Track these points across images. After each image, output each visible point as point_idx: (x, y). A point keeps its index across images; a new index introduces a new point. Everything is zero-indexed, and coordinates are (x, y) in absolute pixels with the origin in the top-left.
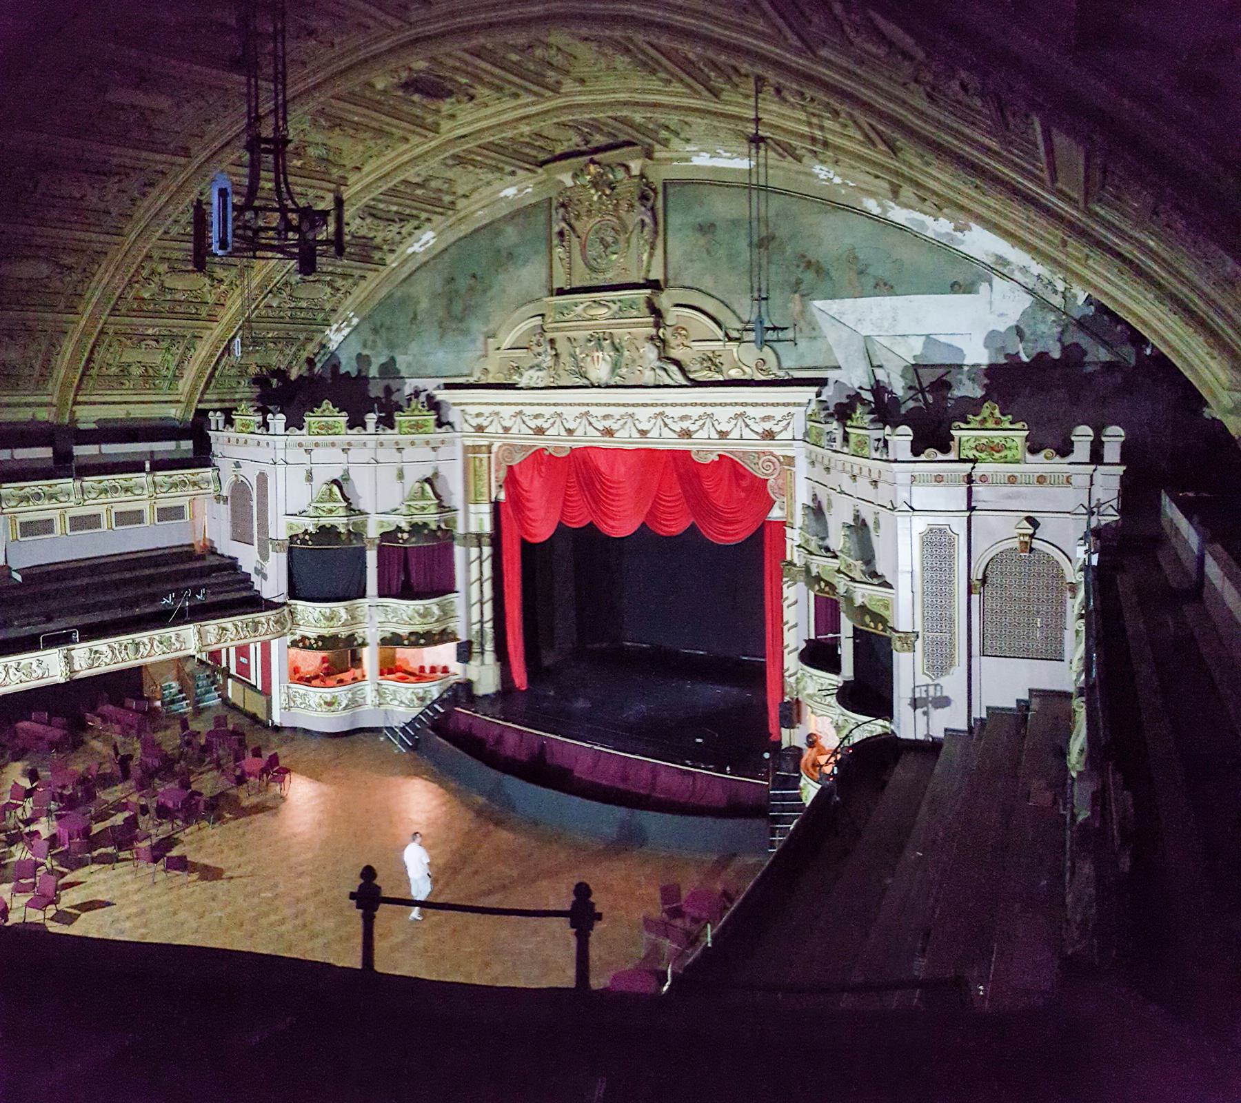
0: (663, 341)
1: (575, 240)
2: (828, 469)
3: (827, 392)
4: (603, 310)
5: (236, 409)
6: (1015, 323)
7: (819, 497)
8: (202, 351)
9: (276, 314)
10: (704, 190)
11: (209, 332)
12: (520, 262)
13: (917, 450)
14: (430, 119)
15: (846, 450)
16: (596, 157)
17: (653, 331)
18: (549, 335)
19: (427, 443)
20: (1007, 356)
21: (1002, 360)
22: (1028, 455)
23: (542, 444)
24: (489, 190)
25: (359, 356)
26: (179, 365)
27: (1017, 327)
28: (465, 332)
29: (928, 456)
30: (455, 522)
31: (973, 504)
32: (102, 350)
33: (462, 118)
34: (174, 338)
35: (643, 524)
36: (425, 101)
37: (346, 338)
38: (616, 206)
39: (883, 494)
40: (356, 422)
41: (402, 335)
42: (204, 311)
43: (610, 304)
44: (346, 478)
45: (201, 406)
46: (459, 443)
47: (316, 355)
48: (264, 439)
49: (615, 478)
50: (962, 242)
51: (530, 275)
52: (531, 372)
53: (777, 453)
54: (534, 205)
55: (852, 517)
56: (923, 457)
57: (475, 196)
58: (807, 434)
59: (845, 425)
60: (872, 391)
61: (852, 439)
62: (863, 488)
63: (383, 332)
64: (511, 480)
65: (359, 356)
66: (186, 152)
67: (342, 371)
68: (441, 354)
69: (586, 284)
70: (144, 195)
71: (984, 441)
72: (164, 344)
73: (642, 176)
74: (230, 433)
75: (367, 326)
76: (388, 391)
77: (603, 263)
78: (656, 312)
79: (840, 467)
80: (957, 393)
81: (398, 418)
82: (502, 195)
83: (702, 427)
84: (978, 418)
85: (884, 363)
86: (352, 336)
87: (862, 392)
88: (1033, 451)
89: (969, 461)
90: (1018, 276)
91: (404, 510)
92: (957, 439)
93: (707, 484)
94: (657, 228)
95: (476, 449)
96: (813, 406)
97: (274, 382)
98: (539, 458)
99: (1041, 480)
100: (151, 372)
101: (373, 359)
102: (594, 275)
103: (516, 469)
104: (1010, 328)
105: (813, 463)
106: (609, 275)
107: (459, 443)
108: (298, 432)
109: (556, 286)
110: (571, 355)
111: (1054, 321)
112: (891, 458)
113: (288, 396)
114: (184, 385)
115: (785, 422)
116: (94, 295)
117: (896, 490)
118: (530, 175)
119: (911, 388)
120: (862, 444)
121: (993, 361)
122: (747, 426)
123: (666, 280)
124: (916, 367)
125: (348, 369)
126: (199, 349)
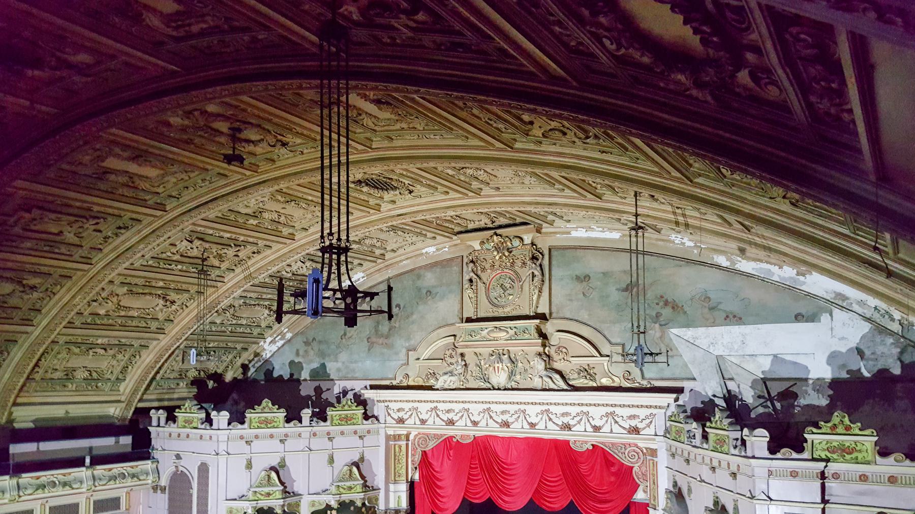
0: (549, 356)
1: (480, 285)
2: (688, 461)
3: (684, 398)
4: (503, 334)
5: (179, 407)
6: (853, 345)
7: (679, 484)
8: (147, 358)
9: (219, 329)
10: (580, 253)
11: (155, 343)
12: (437, 298)
13: (773, 448)
14: (372, 202)
15: (705, 446)
16: (499, 231)
17: (541, 349)
18: (460, 351)
19: (355, 432)
20: (848, 372)
21: (844, 375)
22: (878, 457)
23: (450, 433)
24: (413, 247)
25: (292, 363)
26: (124, 370)
27: (857, 348)
28: (390, 346)
29: (784, 454)
30: (377, 499)
31: (826, 498)
32: (49, 357)
33: (399, 204)
34: (121, 347)
35: (531, 501)
36: (372, 191)
37: (279, 349)
38: (513, 263)
39: (742, 485)
40: (293, 416)
41: (333, 347)
42: (154, 325)
43: (509, 330)
44: (283, 464)
45: (141, 405)
46: (382, 432)
47: (250, 362)
48: (207, 433)
49: (509, 461)
50: (804, 283)
51: (446, 307)
52: (446, 377)
53: (641, 445)
54: (452, 259)
55: (712, 503)
56: (779, 455)
57: (401, 251)
58: (667, 431)
59: (704, 426)
60: (724, 398)
61: (711, 437)
62: (722, 478)
63: (315, 344)
64: (425, 463)
65: (292, 363)
66: (161, 207)
67: (275, 375)
68: (368, 363)
69: (490, 315)
70: (117, 235)
71: (835, 444)
72: (111, 352)
73: (533, 244)
74: (172, 428)
75: (300, 339)
76: (318, 390)
77: (502, 301)
78: (543, 336)
79: (699, 459)
80: (802, 401)
81: (330, 412)
82: (424, 251)
83: (579, 422)
84: (829, 425)
85: (735, 377)
86: (286, 347)
87: (716, 400)
88: (884, 453)
89: (821, 460)
90: (856, 307)
91: (333, 490)
92: (809, 442)
93: (584, 468)
94: (544, 277)
95: (397, 438)
96: (673, 408)
97: (211, 384)
98: (448, 444)
99: (892, 480)
100: (95, 375)
101: (304, 365)
102: (495, 309)
103: (430, 455)
104: (850, 350)
105: (673, 455)
106: (506, 310)
107: (382, 432)
108: (240, 426)
109: (465, 316)
110: (477, 365)
111: (892, 344)
112: (749, 454)
113: (231, 395)
114: (126, 388)
115: (648, 421)
116: (52, 309)
117: (754, 482)
118: (448, 239)
119: (759, 397)
120: (721, 441)
121: (837, 375)
122: (616, 422)
123: (551, 314)
124: (764, 381)
125: (281, 373)
126: (144, 357)
